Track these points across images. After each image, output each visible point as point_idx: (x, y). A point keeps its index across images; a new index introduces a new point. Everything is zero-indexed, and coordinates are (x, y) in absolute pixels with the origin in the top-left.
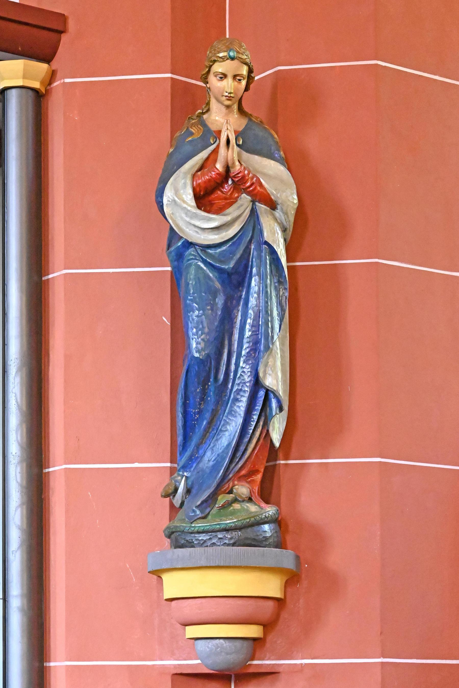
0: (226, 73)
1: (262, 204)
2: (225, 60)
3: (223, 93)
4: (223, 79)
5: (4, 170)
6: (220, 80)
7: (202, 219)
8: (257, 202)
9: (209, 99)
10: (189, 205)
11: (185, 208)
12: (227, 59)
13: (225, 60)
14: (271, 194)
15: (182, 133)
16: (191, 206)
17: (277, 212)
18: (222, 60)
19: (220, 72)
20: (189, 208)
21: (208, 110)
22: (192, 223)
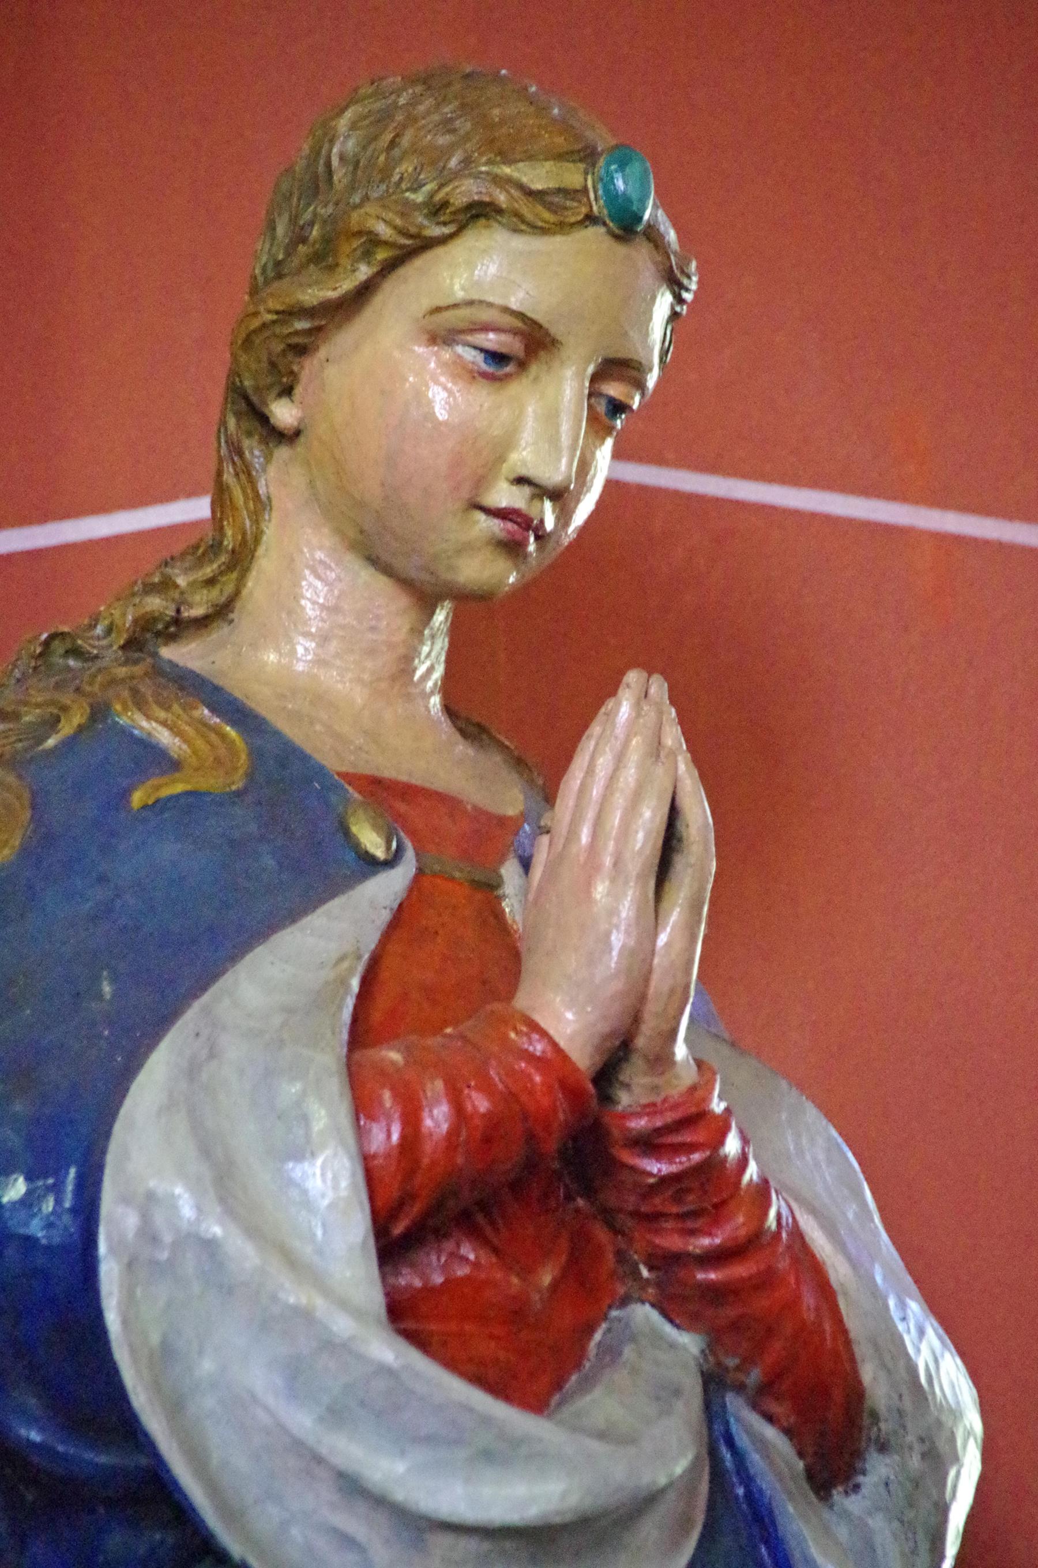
0: (556, 330)
1: (770, 1418)
2: (573, 220)
3: (482, 481)
4: (509, 369)
5: (673, 336)
6: (484, 375)
7: (429, 1440)
8: (740, 1388)
9: (256, 521)
10: (343, 1304)
11: (305, 1315)
12: (591, 219)
13: (572, 225)
14: (862, 1350)
15: (51, 742)
16: (358, 1314)
17: (846, 1515)
18: (547, 215)
19: (514, 305)
20: (342, 1325)
21: (222, 612)
22: (340, 1461)
